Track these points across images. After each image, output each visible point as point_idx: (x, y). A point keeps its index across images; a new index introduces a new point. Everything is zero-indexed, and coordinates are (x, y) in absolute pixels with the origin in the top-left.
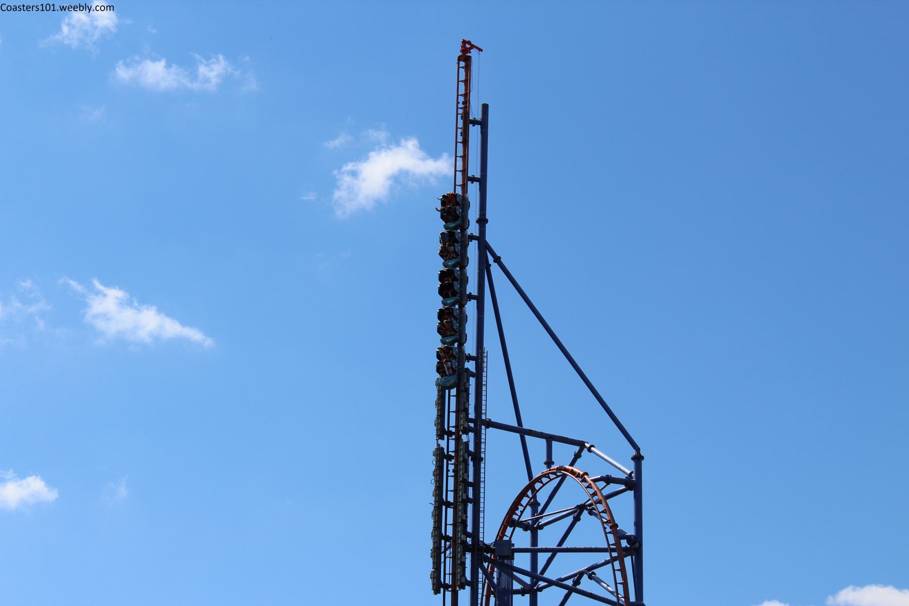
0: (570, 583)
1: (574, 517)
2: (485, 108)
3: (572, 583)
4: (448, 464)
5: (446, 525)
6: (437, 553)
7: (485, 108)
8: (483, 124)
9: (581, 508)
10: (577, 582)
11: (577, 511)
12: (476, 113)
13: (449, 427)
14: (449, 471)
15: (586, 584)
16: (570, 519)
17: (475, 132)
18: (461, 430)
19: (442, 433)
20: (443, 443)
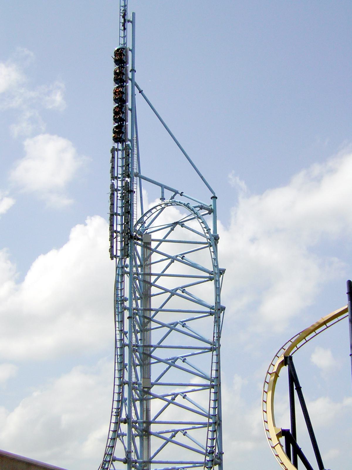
0: (169, 398)
1: (171, 260)
2: (134, 14)
3: (171, 399)
4: (117, 193)
5: (117, 250)
6: (112, 238)
7: (134, 14)
8: (133, 22)
9: (176, 223)
10: (173, 399)
11: (173, 225)
12: (129, 17)
13: (117, 187)
14: (118, 196)
15: (179, 438)
16: (169, 229)
17: (129, 26)
18: (119, 116)
19: (113, 178)
20: (115, 182)
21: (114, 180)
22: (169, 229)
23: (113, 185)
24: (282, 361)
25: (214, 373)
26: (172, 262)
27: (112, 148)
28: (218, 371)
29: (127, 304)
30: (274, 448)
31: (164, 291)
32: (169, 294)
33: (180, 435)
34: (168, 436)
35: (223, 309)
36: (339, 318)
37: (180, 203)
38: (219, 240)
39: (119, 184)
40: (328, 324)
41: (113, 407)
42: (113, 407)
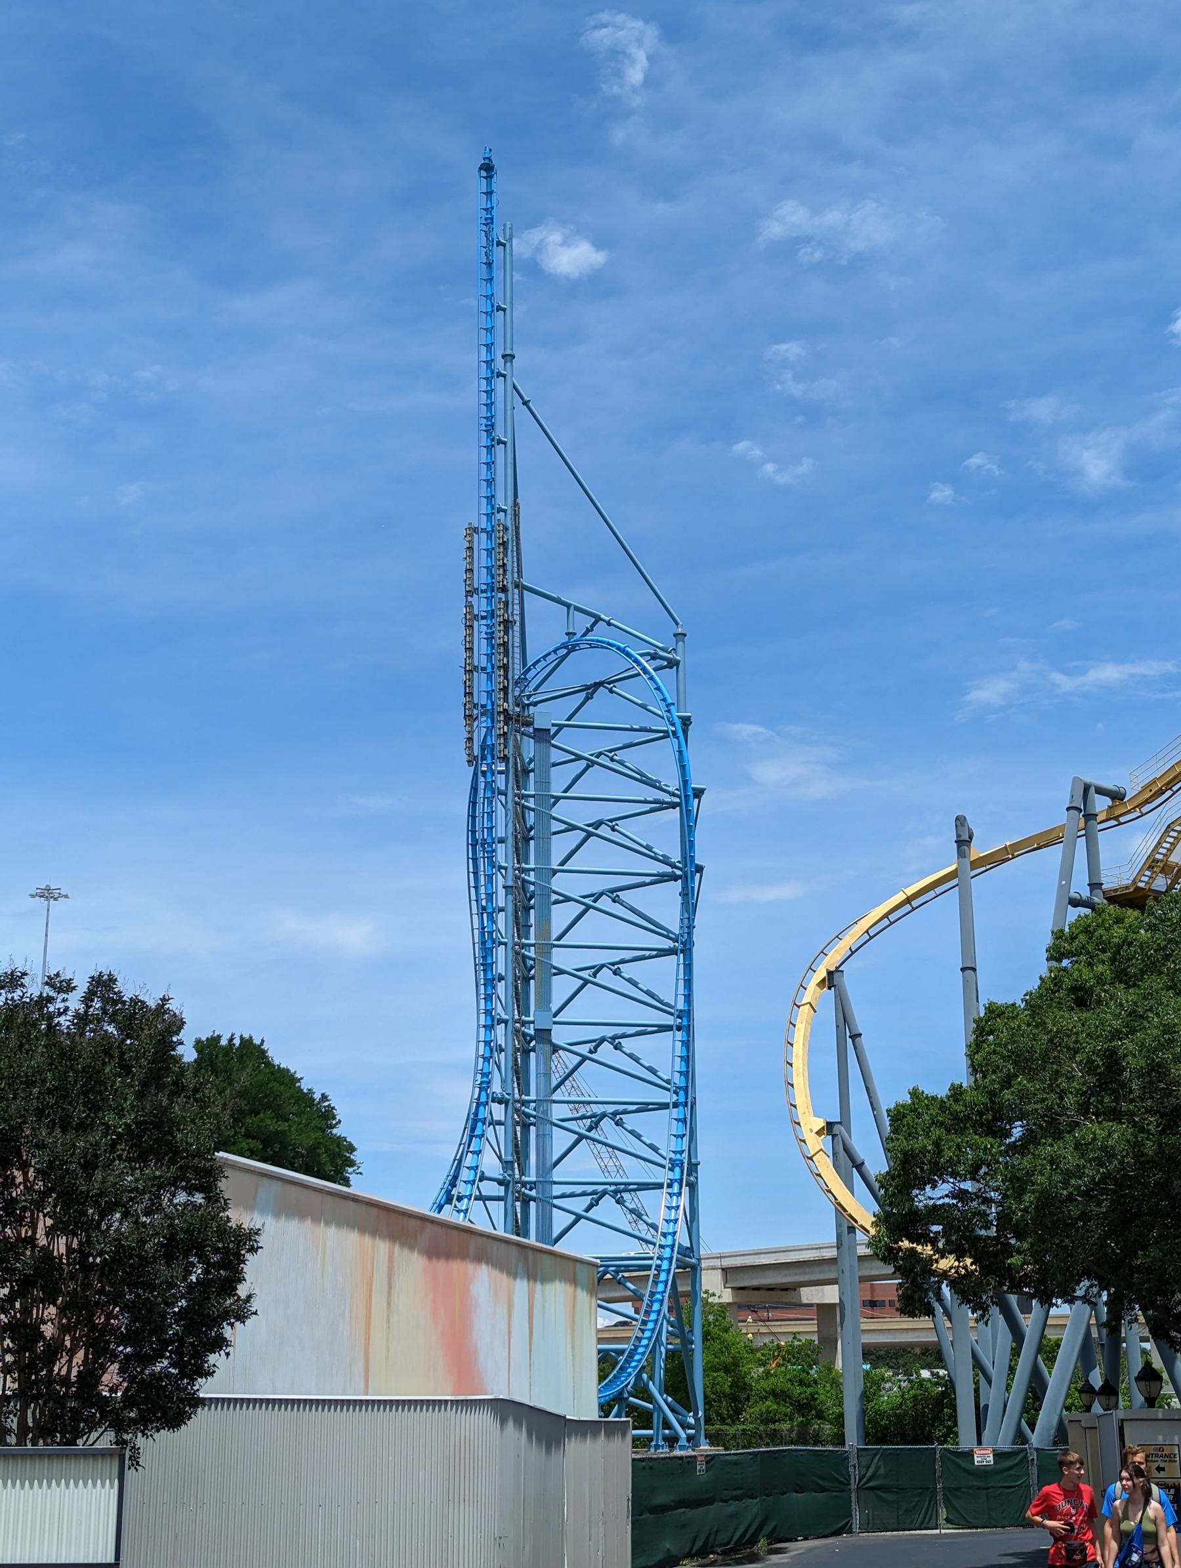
9: (598, 685)
21: (472, 596)
22: (584, 694)
23: (470, 606)
24: (823, 980)
25: (681, 999)
26: (588, 767)
27: (351, 1183)
28: (688, 998)
29: (486, 930)
30: (811, 1158)
31: (573, 757)
32: (583, 764)
33: (606, 1123)
34: (584, 1049)
35: (700, 869)
36: (939, 890)
37: (608, 644)
38: (690, 727)
39: (481, 604)
40: (915, 903)
41: (472, 926)
42: (472, 926)
